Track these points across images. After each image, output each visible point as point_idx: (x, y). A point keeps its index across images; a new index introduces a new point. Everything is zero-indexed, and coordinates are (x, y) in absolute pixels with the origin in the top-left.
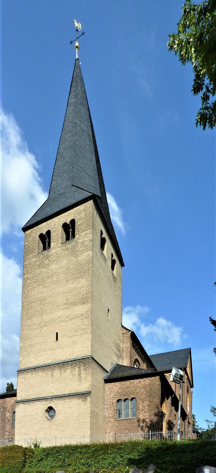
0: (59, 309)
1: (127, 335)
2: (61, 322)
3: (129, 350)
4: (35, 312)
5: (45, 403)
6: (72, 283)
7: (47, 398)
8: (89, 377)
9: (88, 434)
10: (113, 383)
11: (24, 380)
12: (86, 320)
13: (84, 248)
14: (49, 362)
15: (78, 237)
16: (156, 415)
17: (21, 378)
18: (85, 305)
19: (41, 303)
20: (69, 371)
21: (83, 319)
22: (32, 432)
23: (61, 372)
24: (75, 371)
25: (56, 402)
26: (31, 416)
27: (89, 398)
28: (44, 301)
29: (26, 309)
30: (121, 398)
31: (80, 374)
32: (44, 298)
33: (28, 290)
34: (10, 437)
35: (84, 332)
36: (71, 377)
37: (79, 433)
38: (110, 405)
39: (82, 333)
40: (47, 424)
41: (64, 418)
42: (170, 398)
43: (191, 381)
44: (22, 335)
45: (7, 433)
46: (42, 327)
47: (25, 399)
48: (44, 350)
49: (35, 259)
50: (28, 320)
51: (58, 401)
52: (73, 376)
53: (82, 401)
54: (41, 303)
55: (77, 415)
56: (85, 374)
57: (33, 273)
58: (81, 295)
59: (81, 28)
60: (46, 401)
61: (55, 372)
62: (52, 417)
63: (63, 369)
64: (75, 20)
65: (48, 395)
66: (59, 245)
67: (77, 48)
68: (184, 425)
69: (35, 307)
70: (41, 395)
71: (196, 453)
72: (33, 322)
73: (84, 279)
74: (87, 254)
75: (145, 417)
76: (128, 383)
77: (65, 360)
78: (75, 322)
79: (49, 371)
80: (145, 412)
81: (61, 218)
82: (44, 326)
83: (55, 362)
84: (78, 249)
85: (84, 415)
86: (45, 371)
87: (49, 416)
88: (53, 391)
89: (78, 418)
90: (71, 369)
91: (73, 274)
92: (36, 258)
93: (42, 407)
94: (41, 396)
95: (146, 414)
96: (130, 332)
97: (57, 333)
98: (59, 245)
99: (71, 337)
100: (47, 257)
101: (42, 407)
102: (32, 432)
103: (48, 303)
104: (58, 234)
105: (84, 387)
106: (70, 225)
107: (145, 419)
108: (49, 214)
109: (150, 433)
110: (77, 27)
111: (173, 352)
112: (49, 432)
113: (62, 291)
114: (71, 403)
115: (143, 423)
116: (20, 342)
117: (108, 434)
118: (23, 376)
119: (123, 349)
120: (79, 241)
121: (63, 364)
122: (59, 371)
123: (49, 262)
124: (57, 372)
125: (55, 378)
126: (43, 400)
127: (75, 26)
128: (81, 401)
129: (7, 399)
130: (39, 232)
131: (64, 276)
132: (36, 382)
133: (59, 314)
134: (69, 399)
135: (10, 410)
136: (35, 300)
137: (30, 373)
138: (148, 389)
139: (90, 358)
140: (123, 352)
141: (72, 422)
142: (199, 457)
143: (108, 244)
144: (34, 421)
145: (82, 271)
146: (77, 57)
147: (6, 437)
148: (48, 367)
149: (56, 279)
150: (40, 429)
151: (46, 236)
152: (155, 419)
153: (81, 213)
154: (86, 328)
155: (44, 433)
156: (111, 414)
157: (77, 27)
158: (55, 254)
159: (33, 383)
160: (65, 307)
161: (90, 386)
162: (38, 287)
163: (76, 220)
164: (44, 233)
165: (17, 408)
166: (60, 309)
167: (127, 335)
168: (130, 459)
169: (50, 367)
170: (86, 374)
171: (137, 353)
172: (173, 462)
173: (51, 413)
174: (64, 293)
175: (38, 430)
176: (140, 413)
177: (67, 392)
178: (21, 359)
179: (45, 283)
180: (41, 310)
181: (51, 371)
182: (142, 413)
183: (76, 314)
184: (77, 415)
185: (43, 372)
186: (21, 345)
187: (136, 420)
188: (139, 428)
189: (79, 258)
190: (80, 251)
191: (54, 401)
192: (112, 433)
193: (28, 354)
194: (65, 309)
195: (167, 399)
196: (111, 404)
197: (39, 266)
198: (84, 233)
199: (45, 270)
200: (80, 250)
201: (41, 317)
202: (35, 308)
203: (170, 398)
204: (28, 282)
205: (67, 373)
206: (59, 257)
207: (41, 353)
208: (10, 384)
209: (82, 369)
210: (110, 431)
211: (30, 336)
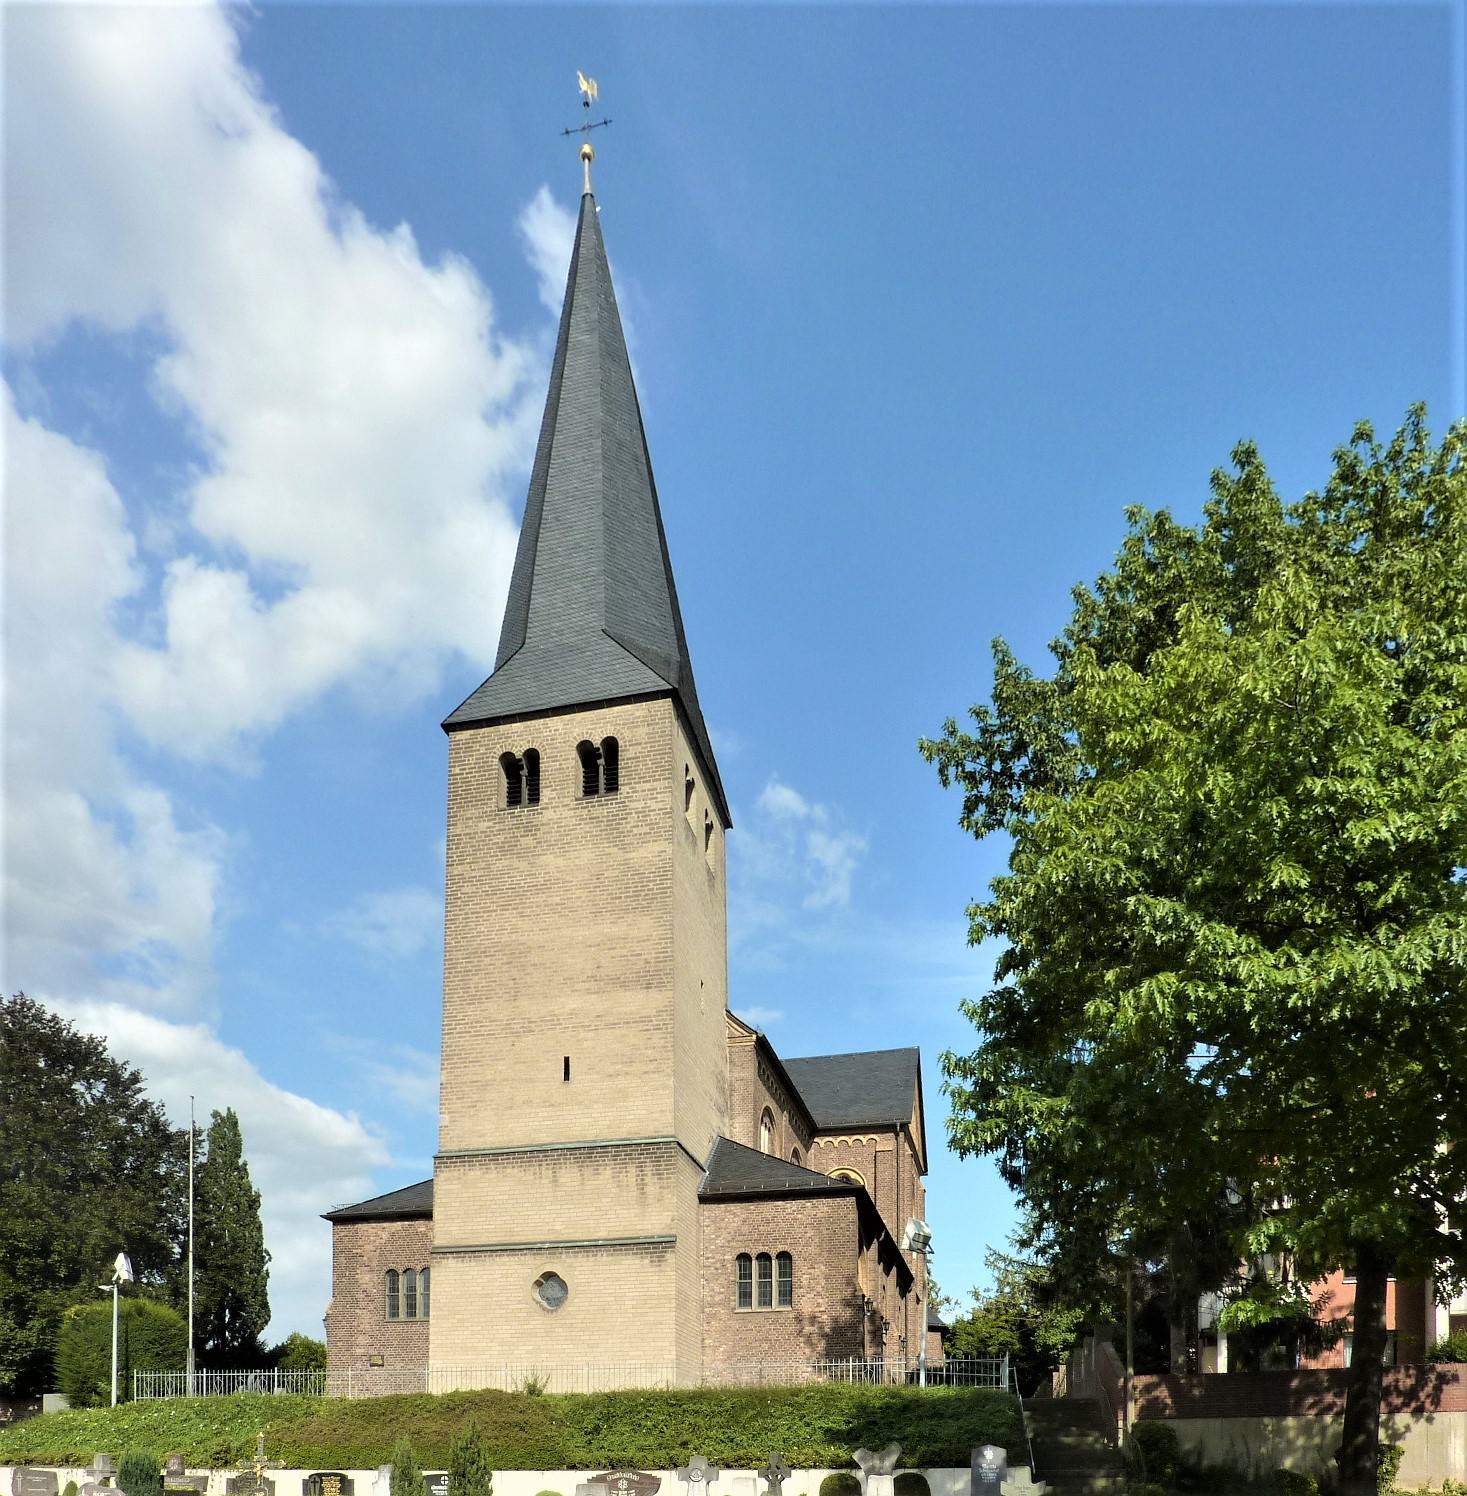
0: (573, 991)
2: (581, 1030)
3: (751, 1089)
4: (494, 984)
6: (611, 923)
7: (539, 1245)
9: (670, 1357)
10: (722, 1206)
11: (459, 1186)
12: (657, 1035)
13: (646, 829)
14: (543, 1138)
15: (628, 793)
16: (847, 1303)
17: (447, 1180)
18: (653, 993)
19: (511, 962)
20: (609, 1172)
21: (647, 1030)
22: (490, 1344)
23: (582, 1175)
25: (568, 1260)
26: (486, 1296)
27: (670, 1256)
28: (520, 957)
29: (460, 972)
30: (747, 1251)
31: (642, 1186)
32: (521, 947)
33: (466, 914)
34: (372, 1351)
35: (652, 1067)
36: (613, 1190)
37: (641, 1353)
38: (717, 1269)
39: (645, 1068)
40: (540, 1321)
41: (596, 1308)
42: (875, 1246)
43: (920, 1154)
44: (447, 1047)
45: (361, 1338)
46: (517, 1034)
47: (464, 1244)
48: (528, 1102)
49: (487, 824)
50: (468, 1004)
51: (576, 1257)
52: (621, 1191)
53: (652, 1262)
54: (511, 962)
55: (635, 1302)
56: (658, 1186)
57: (483, 865)
58: (642, 962)
59: (596, 94)
60: (534, 1254)
61: (563, 1171)
62: (556, 1302)
65: (543, 1238)
66: (567, 801)
67: (587, 161)
68: (903, 1308)
69: (492, 970)
70: (519, 1235)
71: (965, 1420)
72: (485, 1014)
73: (648, 917)
74: (655, 848)
75: (817, 1309)
76: (768, 1208)
77: (595, 1141)
78: (624, 1036)
79: (543, 1168)
81: (572, 724)
82: (524, 1032)
83: (561, 1143)
84: (629, 826)
85: (656, 1302)
87: (543, 1297)
88: (557, 1228)
89: (639, 1310)
92: (491, 824)
93: (522, 1271)
94: (516, 1239)
95: (820, 1301)
96: (754, 1037)
97: (567, 1060)
98: (567, 801)
99: (611, 1076)
100: (530, 829)
101: (522, 1271)
102: (490, 1344)
103: (535, 965)
104: (561, 771)
105: (654, 1224)
106: (601, 751)
107: (817, 1314)
108: (534, 703)
109: (851, 1364)
110: (586, 92)
111: (861, 1054)
112: (550, 1347)
113: (580, 938)
114: (616, 1267)
115: (813, 1325)
116: (442, 1069)
117: (709, 1351)
118: (456, 1174)
119: (731, 1085)
120: (632, 805)
121: (588, 1153)
122: (576, 1170)
123: (538, 843)
124: (569, 1174)
126: (525, 1252)
127: (581, 92)
128: (647, 1261)
129: (363, 1227)
130: (501, 747)
131: (587, 896)
132: (501, 1197)
133: (573, 1003)
135: (374, 1264)
136: (492, 950)
137: (478, 1167)
139: (672, 1145)
140: (731, 1095)
141: (619, 1320)
142: (971, 1427)
143: (701, 792)
144: (498, 1311)
145: (643, 894)
146: (587, 189)
147: (359, 1351)
148: (541, 1155)
150: (516, 1335)
151: (524, 762)
152: (846, 1314)
153: (636, 727)
154: (658, 1057)
155: (531, 1348)
157: (586, 92)
158: (556, 826)
159: (489, 1198)
160: (591, 985)
161: (673, 1220)
162: (499, 912)
163: (621, 743)
164: (518, 752)
165: (436, 1269)
166: (576, 991)
168: (828, 1430)
170: (660, 1188)
171: (768, 1089)
172: (922, 1437)
173: (552, 1289)
174: (587, 946)
175: (510, 1339)
177: (602, 1233)
178: (446, 1119)
179: (525, 903)
180: (512, 982)
182: (808, 1296)
183: (626, 1013)
184: (635, 1302)
185: (522, 1169)
186: (443, 1079)
187: (791, 1315)
188: (802, 1339)
189: (633, 855)
190: (636, 835)
191: (563, 1256)
192: (722, 1349)
193: (469, 1107)
194: (591, 993)
195: (868, 1249)
196: (718, 1265)
197: (502, 849)
198: (647, 786)
199: (523, 865)
200: (635, 830)
201: (514, 1004)
202: (492, 973)
203: (875, 1246)
204: (464, 890)
205: (601, 1177)
206: (569, 837)
207: (514, 1112)
208: (224, 1114)
209: (649, 1173)
210: (717, 1344)
211: (475, 1055)
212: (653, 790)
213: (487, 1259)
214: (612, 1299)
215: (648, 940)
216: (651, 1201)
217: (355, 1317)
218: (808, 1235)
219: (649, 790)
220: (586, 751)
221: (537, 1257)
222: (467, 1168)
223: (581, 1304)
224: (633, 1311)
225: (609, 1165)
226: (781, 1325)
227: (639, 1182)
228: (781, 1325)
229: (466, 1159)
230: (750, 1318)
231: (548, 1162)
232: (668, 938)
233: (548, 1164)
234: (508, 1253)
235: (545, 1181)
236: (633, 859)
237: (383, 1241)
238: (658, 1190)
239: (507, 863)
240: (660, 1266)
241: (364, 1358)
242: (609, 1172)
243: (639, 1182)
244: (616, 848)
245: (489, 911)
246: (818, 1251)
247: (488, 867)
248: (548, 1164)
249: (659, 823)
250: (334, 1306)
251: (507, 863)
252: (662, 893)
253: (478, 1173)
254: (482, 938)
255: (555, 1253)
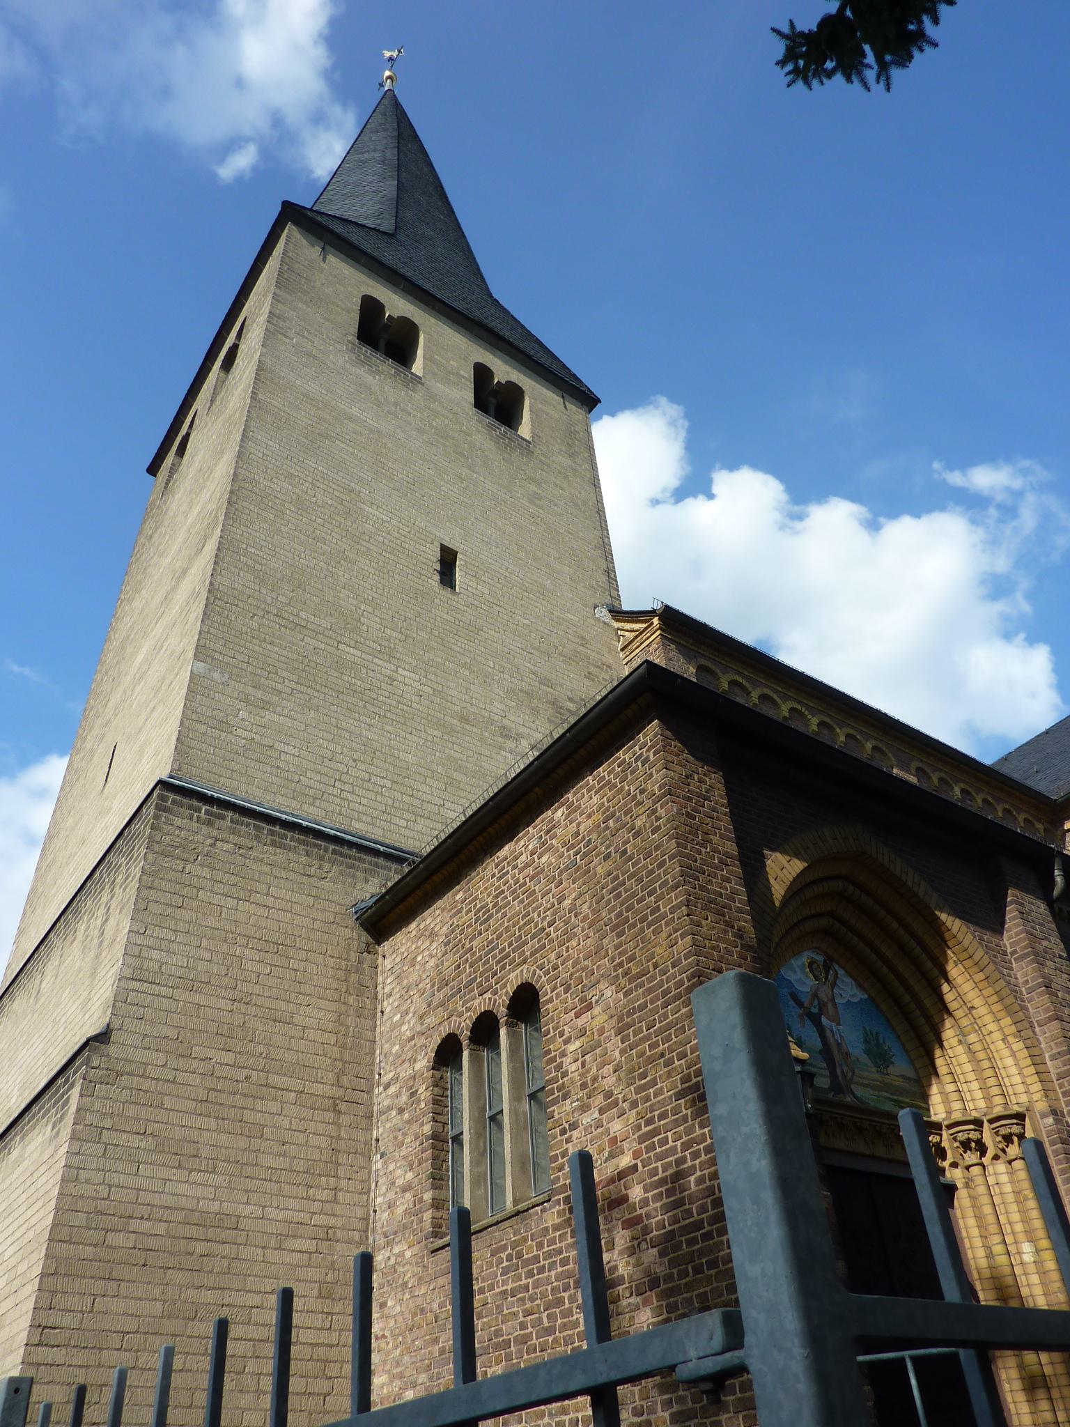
1: (648, 642)
80: (611, 1103)
97: (287, 1297)
138: (600, 870)
149: (603, 813)
167: (648, 642)
176: (574, 1126)
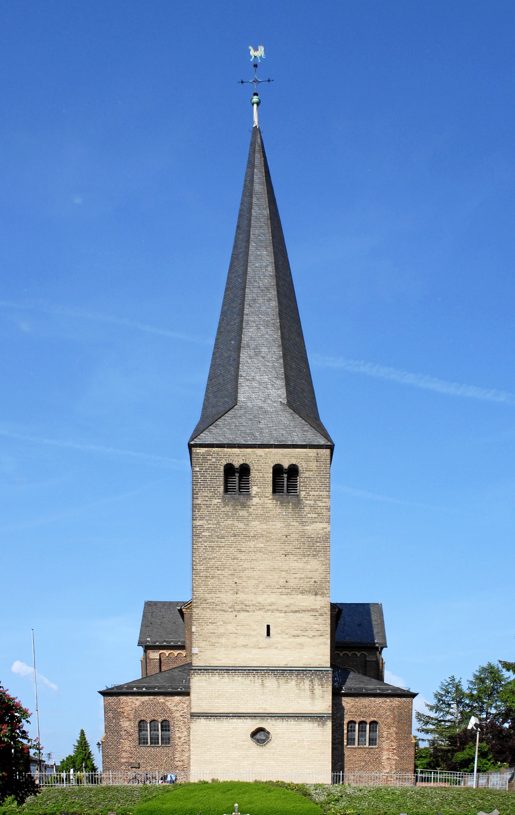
5: (251, 722)
8: (328, 695)
18: (319, 598)
20: (293, 683)
24: (304, 685)
25: (272, 723)
30: (354, 719)
31: (312, 691)
36: (296, 691)
51: (275, 721)
53: (319, 725)
56: (321, 691)
60: (252, 719)
61: (268, 680)
63: (282, 679)
64: (250, 48)
70: (242, 709)
74: (320, 526)
76: (366, 701)
80: (392, 741)
86: (248, 677)
90: (296, 681)
91: (296, 547)
95: (393, 744)
97: (268, 627)
99: (294, 636)
109: (433, 775)
118: (204, 678)
120: (307, 502)
122: (275, 680)
123: (250, 514)
124: (271, 682)
125: (269, 689)
126: (247, 717)
129: (123, 698)
134: (296, 721)
135: (131, 717)
137: (217, 675)
146: (256, 123)
147: (123, 760)
148: (254, 672)
156: (338, 738)
169: (257, 673)
181: (260, 678)
182: (387, 741)
185: (244, 678)
191: (269, 720)
196: (338, 726)
197: (227, 515)
200: (309, 515)
205: (289, 684)
209: (317, 684)
210: (337, 762)
212: (320, 496)
213: (224, 720)
214: (297, 741)
215: (316, 571)
216: (318, 697)
217: (119, 743)
218: (388, 714)
219: (317, 496)
220: (278, 470)
221: (254, 720)
222: (210, 675)
223: (279, 743)
224: (308, 747)
225: (294, 679)
226: (372, 754)
227: (311, 688)
228: (372, 754)
229: (210, 671)
230: (354, 751)
231: (258, 675)
232: (327, 572)
233: (258, 677)
234: (237, 717)
235: (256, 684)
236: (307, 529)
237: (137, 706)
238: (321, 692)
239: (231, 522)
240: (323, 727)
241: (126, 764)
242: (293, 683)
243: (311, 688)
244: (298, 523)
245: (220, 547)
246: (392, 721)
247: (218, 523)
248: (258, 677)
249: (323, 513)
250: (106, 738)
251: (231, 522)
252: (326, 551)
253: (217, 678)
254: (216, 560)
255: (264, 719)
